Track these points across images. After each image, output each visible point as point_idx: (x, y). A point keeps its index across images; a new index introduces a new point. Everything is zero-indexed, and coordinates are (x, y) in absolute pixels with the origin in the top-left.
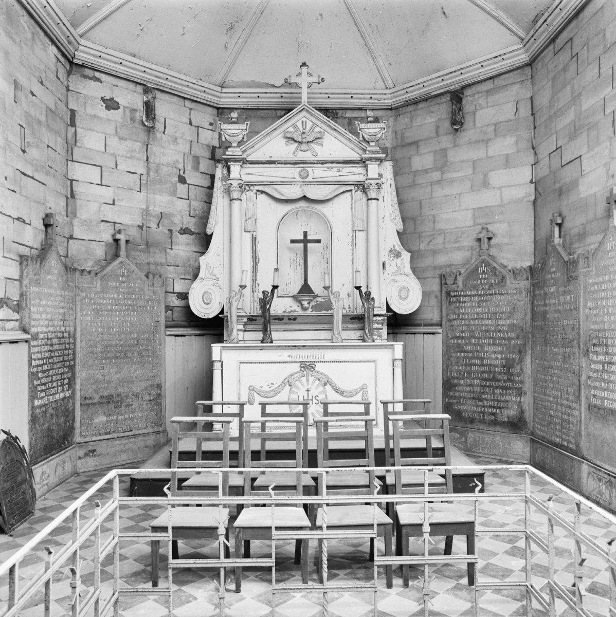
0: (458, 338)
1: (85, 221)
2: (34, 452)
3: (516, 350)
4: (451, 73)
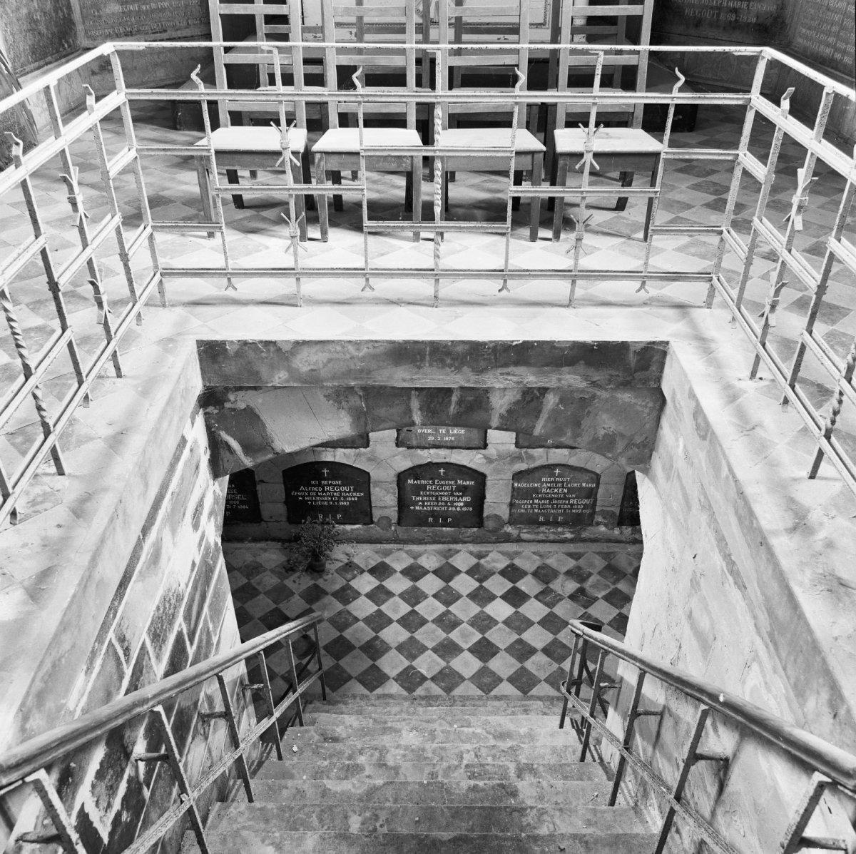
2: (16, 55)
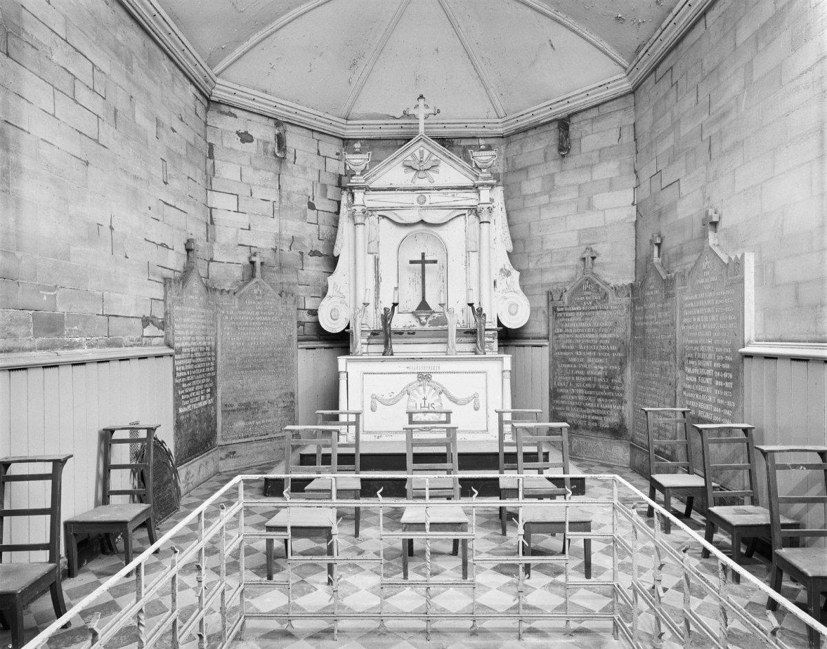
0: (563, 350)
1: (224, 245)
2: (179, 455)
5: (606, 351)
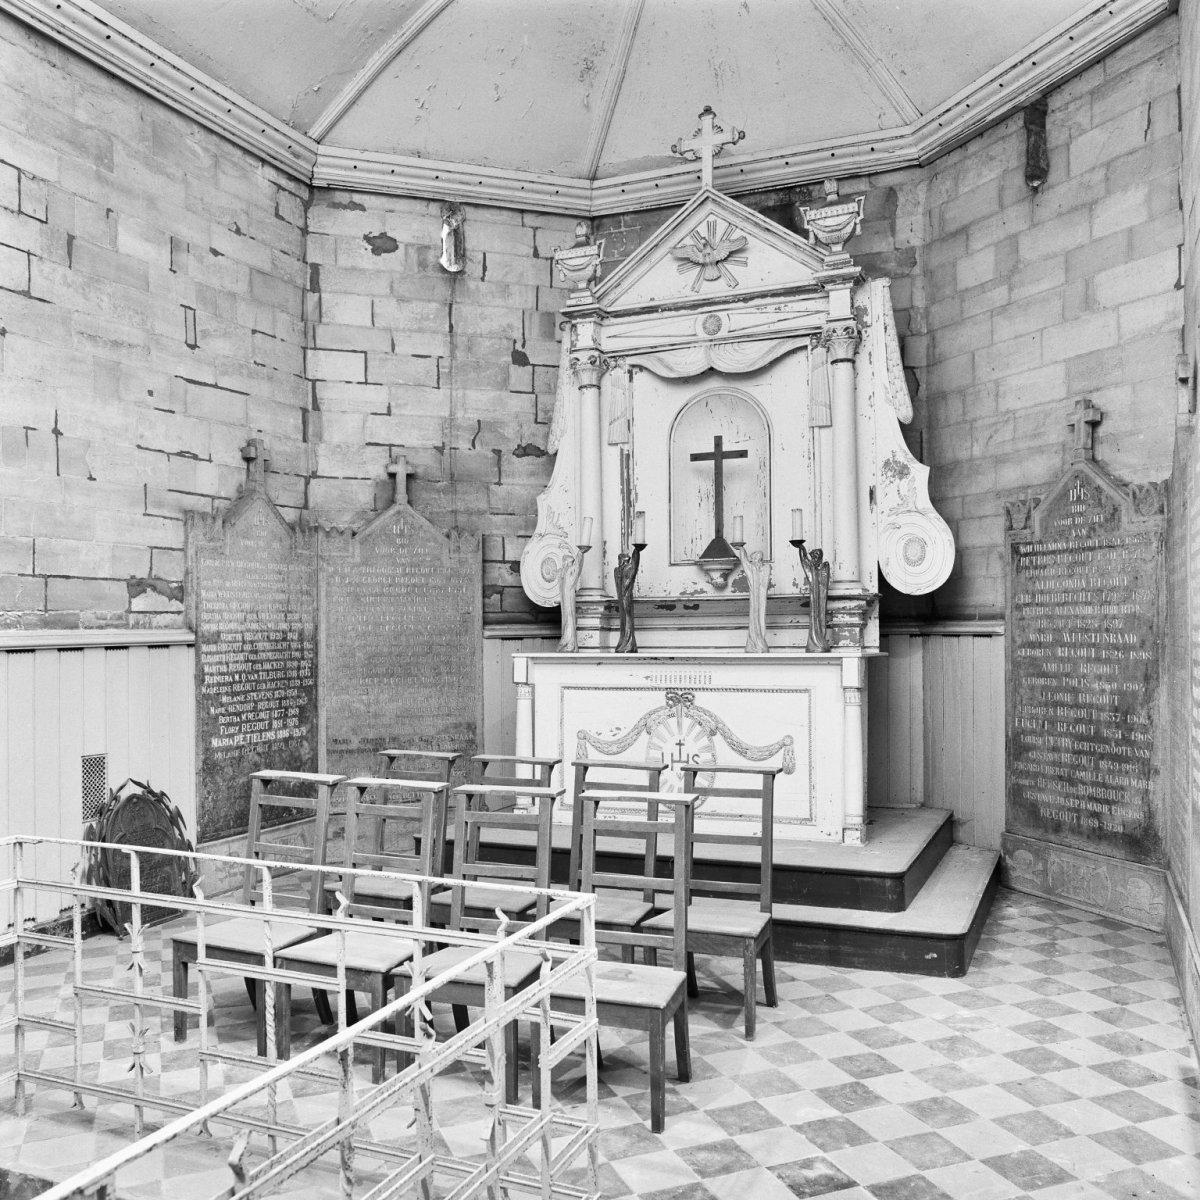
0: (1032, 645)
1: (339, 446)
3: (1140, 674)
4: (1015, 66)
5: (1116, 647)
